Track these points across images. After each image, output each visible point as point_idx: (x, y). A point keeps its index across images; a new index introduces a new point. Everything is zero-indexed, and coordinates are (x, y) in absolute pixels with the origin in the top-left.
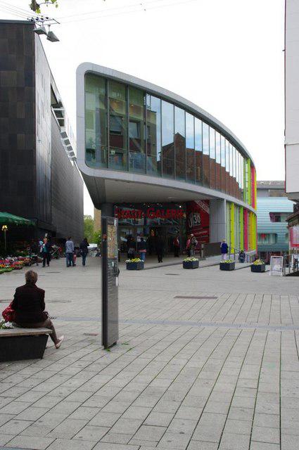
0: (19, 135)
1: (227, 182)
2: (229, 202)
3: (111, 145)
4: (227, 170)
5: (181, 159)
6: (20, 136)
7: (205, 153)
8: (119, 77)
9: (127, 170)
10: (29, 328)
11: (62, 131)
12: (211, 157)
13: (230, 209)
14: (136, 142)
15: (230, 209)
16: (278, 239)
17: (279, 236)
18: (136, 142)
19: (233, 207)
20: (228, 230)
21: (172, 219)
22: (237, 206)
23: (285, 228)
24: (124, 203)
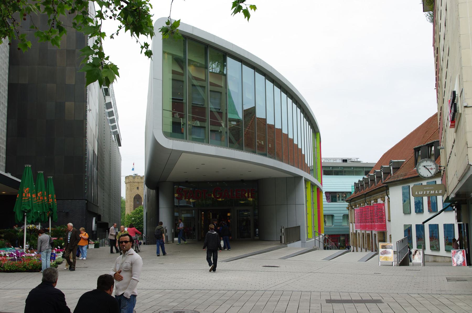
0: (67, 103)
1: (291, 152)
2: (306, 181)
3: (210, 118)
4: (295, 142)
5: (252, 132)
6: (69, 105)
7: (278, 126)
8: (246, 56)
9: (240, 148)
10: (17, 178)
11: (107, 102)
12: (276, 127)
13: (313, 191)
14: (216, 115)
15: (313, 191)
16: (335, 221)
17: (335, 218)
18: (216, 115)
19: (309, 186)
20: (306, 225)
21: (229, 201)
22: (313, 185)
23: (346, 209)
24: (187, 182)
